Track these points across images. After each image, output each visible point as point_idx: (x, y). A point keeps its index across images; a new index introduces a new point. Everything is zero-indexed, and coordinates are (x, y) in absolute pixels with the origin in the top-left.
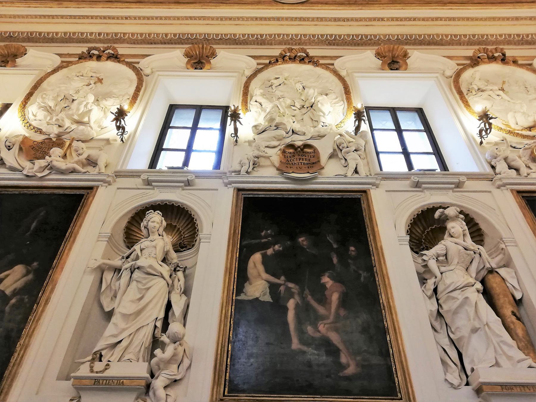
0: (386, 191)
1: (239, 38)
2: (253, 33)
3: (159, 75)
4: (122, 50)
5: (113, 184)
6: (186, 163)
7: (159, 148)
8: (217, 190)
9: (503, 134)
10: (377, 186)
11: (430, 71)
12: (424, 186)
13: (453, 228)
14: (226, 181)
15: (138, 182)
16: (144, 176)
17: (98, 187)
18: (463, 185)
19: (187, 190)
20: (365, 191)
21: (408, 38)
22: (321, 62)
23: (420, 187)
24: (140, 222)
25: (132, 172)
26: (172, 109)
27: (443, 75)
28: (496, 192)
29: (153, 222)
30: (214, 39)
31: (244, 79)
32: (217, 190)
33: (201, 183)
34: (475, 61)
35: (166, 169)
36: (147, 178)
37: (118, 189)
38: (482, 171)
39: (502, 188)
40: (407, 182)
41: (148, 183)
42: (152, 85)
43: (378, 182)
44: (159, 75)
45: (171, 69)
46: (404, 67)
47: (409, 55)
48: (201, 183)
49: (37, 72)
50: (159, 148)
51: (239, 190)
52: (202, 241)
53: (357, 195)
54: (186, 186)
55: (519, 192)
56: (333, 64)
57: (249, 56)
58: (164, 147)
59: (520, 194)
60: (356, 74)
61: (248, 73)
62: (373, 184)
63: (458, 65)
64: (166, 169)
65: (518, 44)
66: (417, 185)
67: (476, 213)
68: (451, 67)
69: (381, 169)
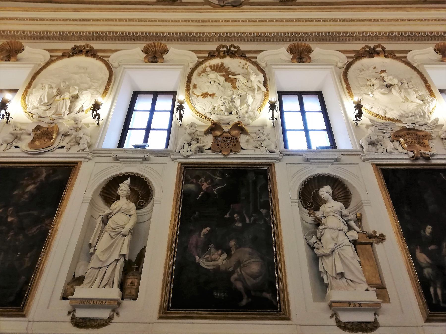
0: (287, 164)
1: (27, 34)
2: (77, 30)
3: (124, 68)
4: (96, 45)
5: (92, 159)
6: (146, 141)
7: (126, 128)
8: (167, 163)
9: (370, 116)
10: (280, 160)
11: (328, 64)
12: (311, 161)
13: (323, 195)
14: (173, 157)
15: (299, 159)
16: (114, 154)
17: (81, 162)
18: (340, 159)
19: (144, 163)
20: (270, 165)
21: (221, 35)
22: (397, 55)
23: (309, 161)
24: (116, 191)
25: (105, 150)
26: (136, 94)
27: (337, 66)
28: (362, 164)
29: (122, 190)
30: (377, 36)
31: (189, 70)
32: (167, 163)
33: (154, 159)
34: (359, 55)
35: (133, 148)
36: (116, 155)
37: (96, 163)
38: (355, 149)
39: (366, 161)
40: (300, 157)
41: (117, 159)
42: (120, 75)
43: (281, 157)
44: (124, 68)
45: (282, 63)
46: (308, 61)
47: (313, 50)
48: (154, 159)
49: (32, 65)
50: (126, 128)
51: (182, 164)
52: (155, 202)
53: (266, 168)
54: (143, 160)
55: (377, 165)
56: (256, 58)
57: (45, 50)
58: (130, 127)
59: (378, 166)
60: (273, 67)
61: (192, 65)
62: (277, 159)
63: (348, 57)
64: (133, 148)
65: (421, 40)
66: (308, 160)
67: (350, 184)
68: (342, 59)
69: (286, 147)
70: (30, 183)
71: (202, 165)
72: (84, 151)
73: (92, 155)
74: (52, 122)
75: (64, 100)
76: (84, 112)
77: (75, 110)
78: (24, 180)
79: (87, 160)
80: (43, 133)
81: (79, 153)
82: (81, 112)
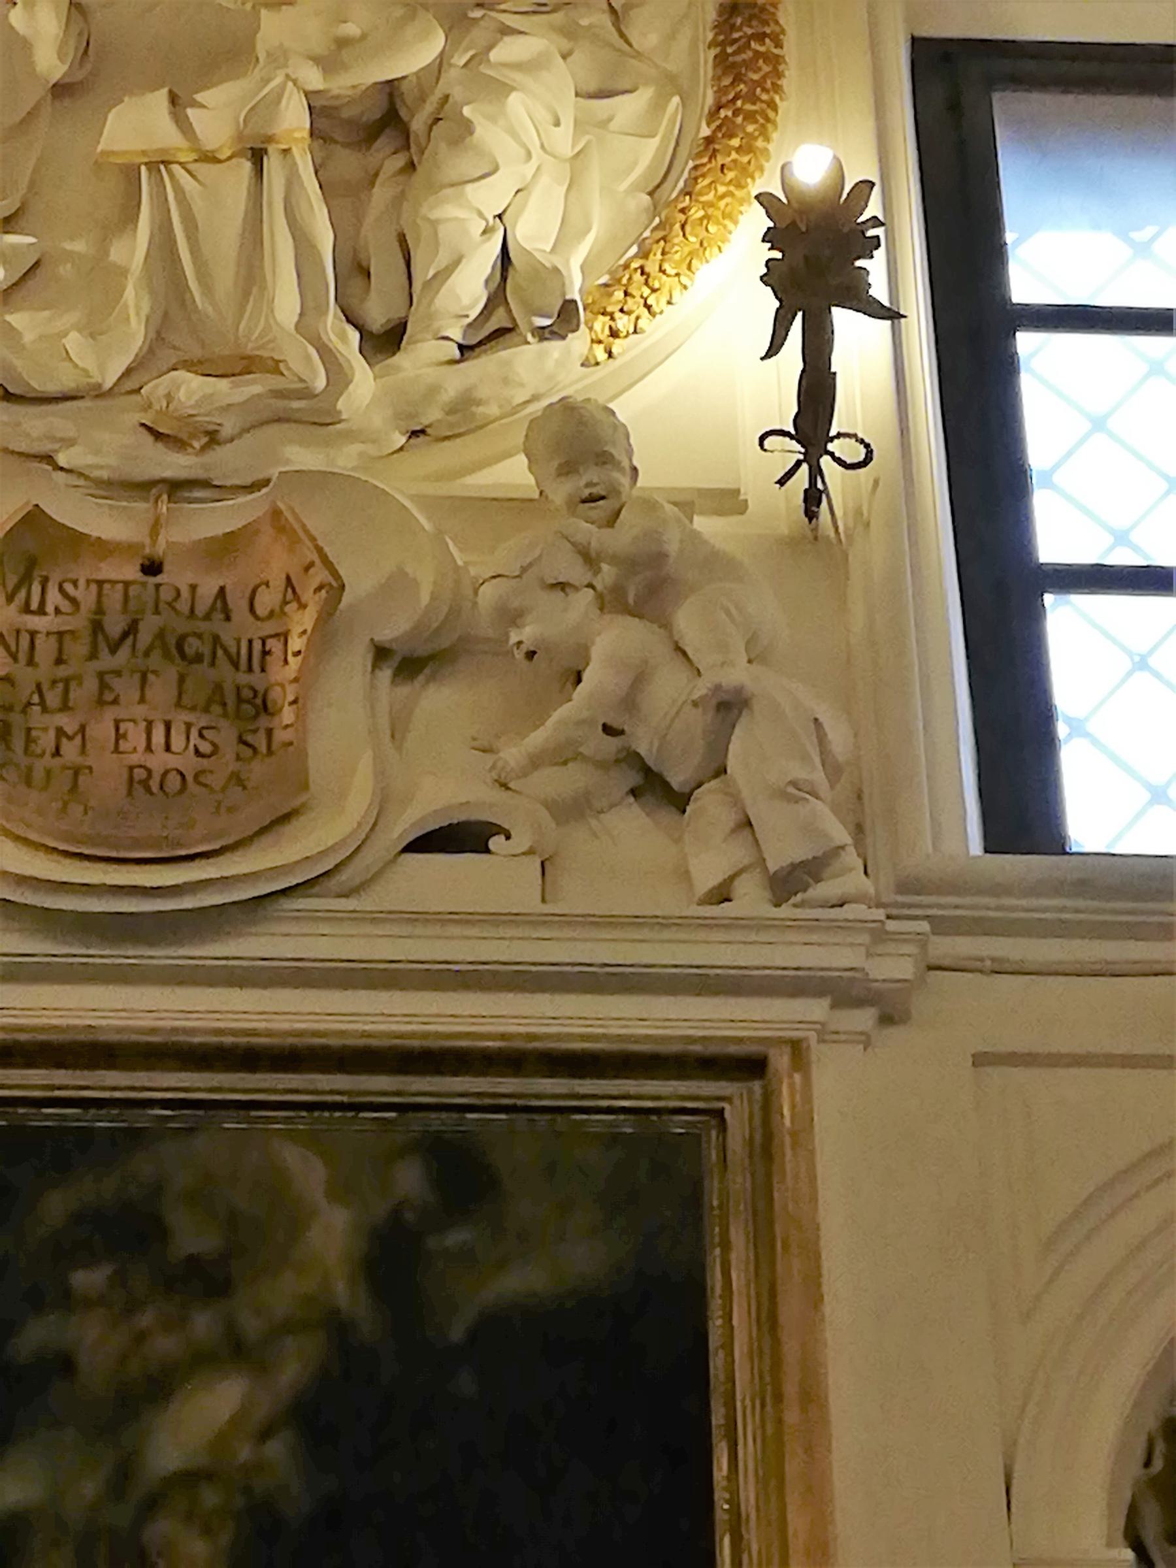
0: (981, 1060)
70: (166, 1345)
71: (92, 1065)
72: (820, 891)
73: (922, 941)
74: (177, 464)
75: (257, 156)
76: (578, 343)
77: (443, 300)
78: (67, 1300)
79: (863, 1019)
80: (97, 627)
81: (735, 924)
82: (543, 334)
